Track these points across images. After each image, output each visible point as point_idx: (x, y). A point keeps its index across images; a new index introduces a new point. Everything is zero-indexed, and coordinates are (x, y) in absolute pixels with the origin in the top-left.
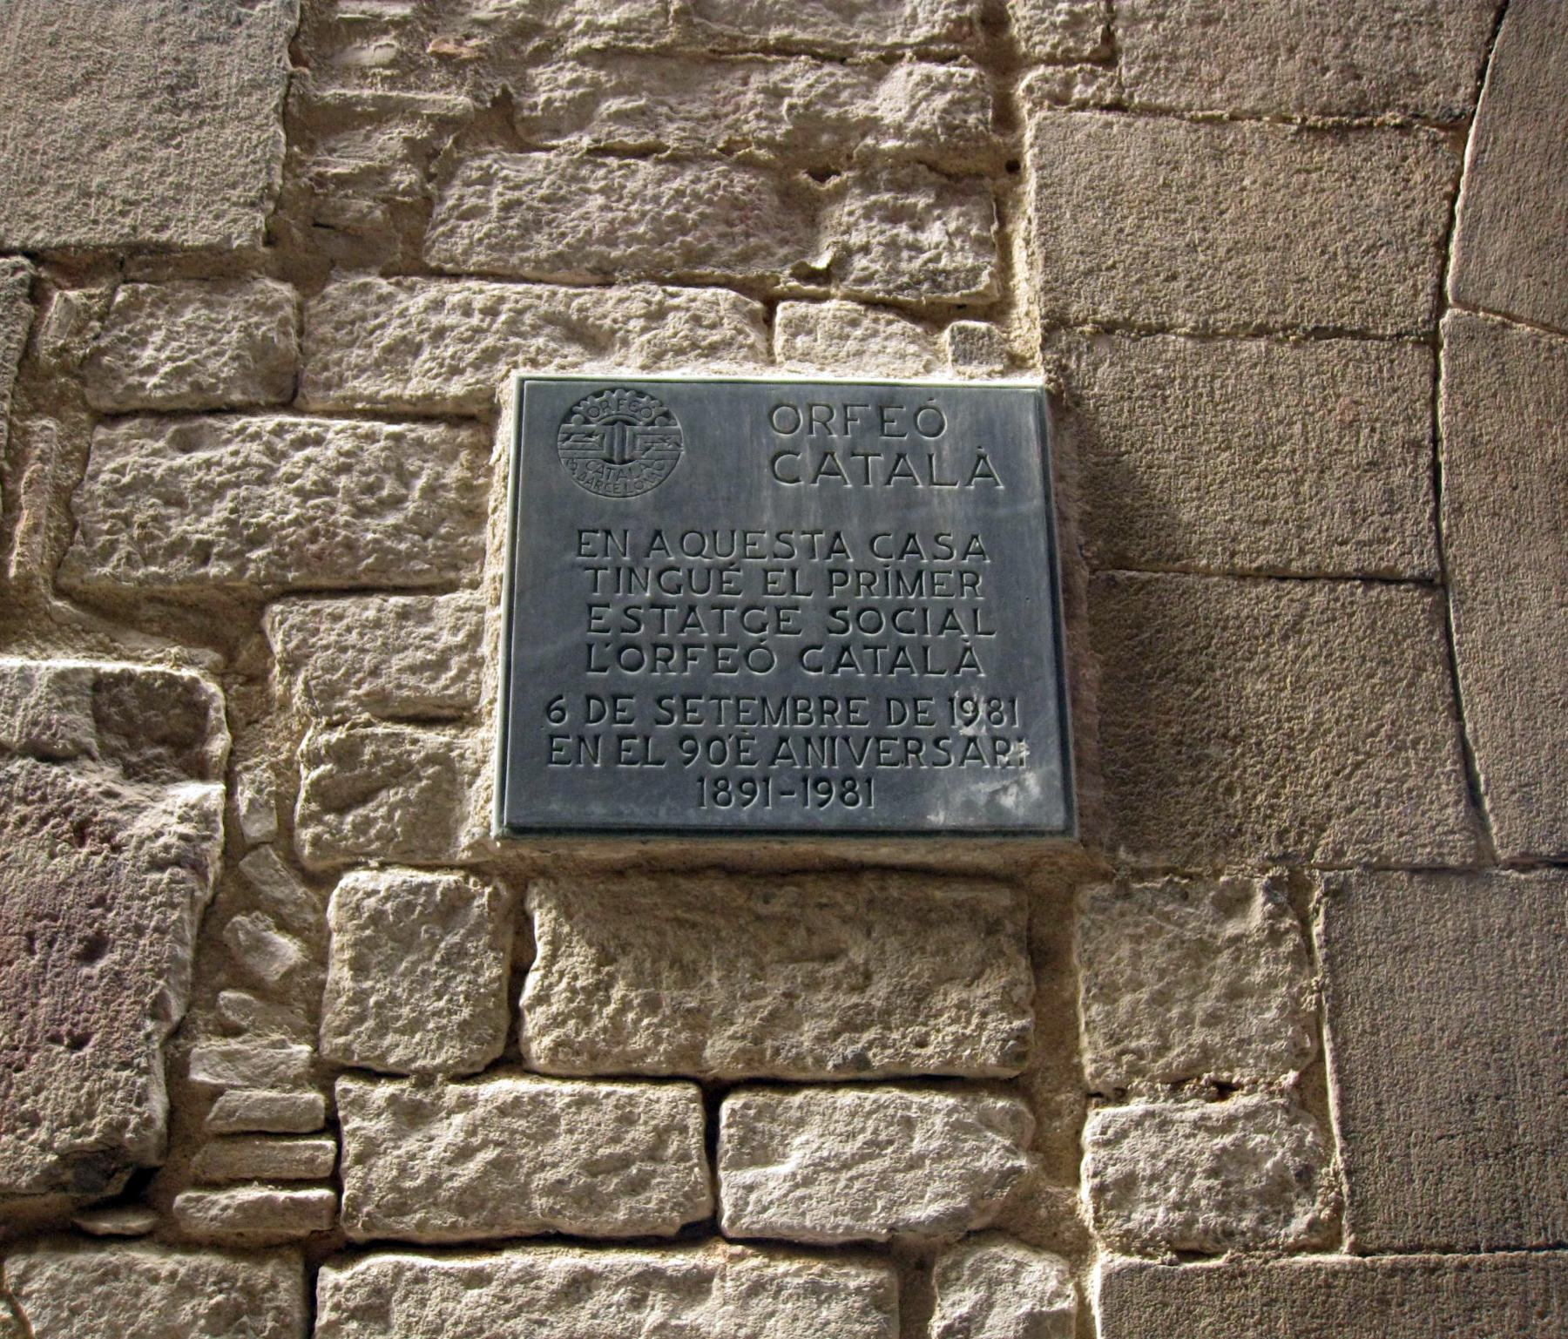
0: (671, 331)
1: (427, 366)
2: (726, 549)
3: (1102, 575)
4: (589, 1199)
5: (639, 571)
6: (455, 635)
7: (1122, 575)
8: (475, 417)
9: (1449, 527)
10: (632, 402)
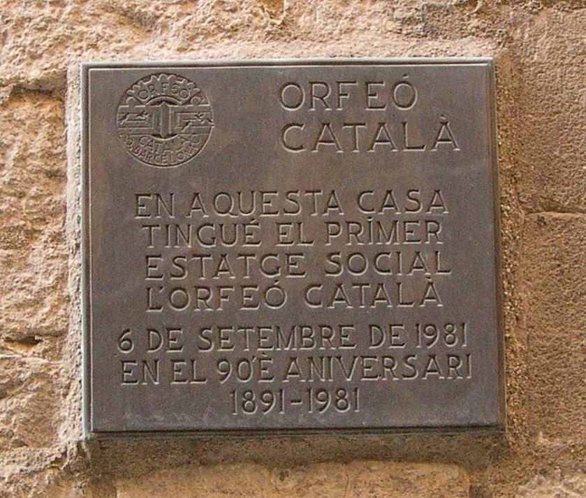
0: (202, 16)
1: (12, 53)
2: (249, 207)
3: (534, 216)
5: (183, 226)
6: (47, 278)
7: (547, 215)
10: (173, 84)
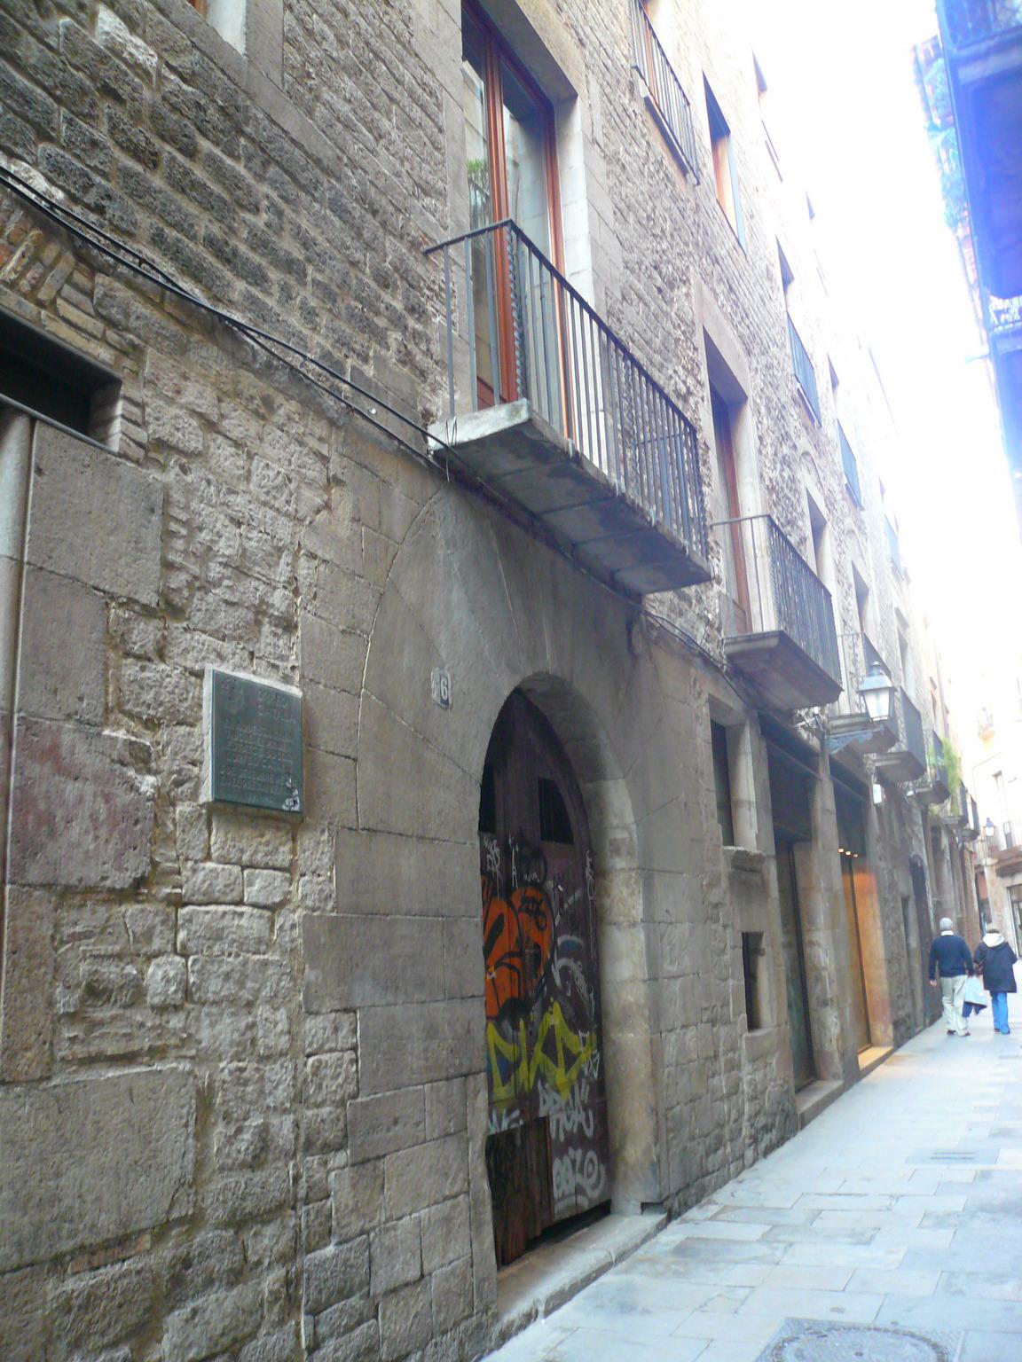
4: (225, 893)
8: (199, 675)
9: (56, 173)
